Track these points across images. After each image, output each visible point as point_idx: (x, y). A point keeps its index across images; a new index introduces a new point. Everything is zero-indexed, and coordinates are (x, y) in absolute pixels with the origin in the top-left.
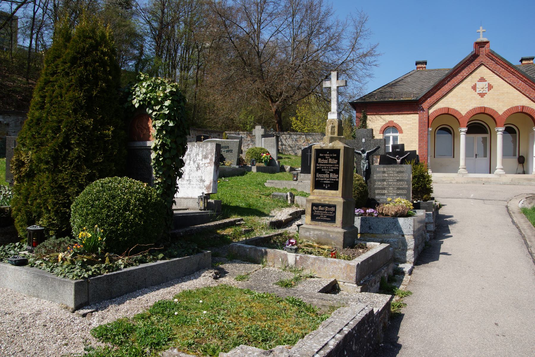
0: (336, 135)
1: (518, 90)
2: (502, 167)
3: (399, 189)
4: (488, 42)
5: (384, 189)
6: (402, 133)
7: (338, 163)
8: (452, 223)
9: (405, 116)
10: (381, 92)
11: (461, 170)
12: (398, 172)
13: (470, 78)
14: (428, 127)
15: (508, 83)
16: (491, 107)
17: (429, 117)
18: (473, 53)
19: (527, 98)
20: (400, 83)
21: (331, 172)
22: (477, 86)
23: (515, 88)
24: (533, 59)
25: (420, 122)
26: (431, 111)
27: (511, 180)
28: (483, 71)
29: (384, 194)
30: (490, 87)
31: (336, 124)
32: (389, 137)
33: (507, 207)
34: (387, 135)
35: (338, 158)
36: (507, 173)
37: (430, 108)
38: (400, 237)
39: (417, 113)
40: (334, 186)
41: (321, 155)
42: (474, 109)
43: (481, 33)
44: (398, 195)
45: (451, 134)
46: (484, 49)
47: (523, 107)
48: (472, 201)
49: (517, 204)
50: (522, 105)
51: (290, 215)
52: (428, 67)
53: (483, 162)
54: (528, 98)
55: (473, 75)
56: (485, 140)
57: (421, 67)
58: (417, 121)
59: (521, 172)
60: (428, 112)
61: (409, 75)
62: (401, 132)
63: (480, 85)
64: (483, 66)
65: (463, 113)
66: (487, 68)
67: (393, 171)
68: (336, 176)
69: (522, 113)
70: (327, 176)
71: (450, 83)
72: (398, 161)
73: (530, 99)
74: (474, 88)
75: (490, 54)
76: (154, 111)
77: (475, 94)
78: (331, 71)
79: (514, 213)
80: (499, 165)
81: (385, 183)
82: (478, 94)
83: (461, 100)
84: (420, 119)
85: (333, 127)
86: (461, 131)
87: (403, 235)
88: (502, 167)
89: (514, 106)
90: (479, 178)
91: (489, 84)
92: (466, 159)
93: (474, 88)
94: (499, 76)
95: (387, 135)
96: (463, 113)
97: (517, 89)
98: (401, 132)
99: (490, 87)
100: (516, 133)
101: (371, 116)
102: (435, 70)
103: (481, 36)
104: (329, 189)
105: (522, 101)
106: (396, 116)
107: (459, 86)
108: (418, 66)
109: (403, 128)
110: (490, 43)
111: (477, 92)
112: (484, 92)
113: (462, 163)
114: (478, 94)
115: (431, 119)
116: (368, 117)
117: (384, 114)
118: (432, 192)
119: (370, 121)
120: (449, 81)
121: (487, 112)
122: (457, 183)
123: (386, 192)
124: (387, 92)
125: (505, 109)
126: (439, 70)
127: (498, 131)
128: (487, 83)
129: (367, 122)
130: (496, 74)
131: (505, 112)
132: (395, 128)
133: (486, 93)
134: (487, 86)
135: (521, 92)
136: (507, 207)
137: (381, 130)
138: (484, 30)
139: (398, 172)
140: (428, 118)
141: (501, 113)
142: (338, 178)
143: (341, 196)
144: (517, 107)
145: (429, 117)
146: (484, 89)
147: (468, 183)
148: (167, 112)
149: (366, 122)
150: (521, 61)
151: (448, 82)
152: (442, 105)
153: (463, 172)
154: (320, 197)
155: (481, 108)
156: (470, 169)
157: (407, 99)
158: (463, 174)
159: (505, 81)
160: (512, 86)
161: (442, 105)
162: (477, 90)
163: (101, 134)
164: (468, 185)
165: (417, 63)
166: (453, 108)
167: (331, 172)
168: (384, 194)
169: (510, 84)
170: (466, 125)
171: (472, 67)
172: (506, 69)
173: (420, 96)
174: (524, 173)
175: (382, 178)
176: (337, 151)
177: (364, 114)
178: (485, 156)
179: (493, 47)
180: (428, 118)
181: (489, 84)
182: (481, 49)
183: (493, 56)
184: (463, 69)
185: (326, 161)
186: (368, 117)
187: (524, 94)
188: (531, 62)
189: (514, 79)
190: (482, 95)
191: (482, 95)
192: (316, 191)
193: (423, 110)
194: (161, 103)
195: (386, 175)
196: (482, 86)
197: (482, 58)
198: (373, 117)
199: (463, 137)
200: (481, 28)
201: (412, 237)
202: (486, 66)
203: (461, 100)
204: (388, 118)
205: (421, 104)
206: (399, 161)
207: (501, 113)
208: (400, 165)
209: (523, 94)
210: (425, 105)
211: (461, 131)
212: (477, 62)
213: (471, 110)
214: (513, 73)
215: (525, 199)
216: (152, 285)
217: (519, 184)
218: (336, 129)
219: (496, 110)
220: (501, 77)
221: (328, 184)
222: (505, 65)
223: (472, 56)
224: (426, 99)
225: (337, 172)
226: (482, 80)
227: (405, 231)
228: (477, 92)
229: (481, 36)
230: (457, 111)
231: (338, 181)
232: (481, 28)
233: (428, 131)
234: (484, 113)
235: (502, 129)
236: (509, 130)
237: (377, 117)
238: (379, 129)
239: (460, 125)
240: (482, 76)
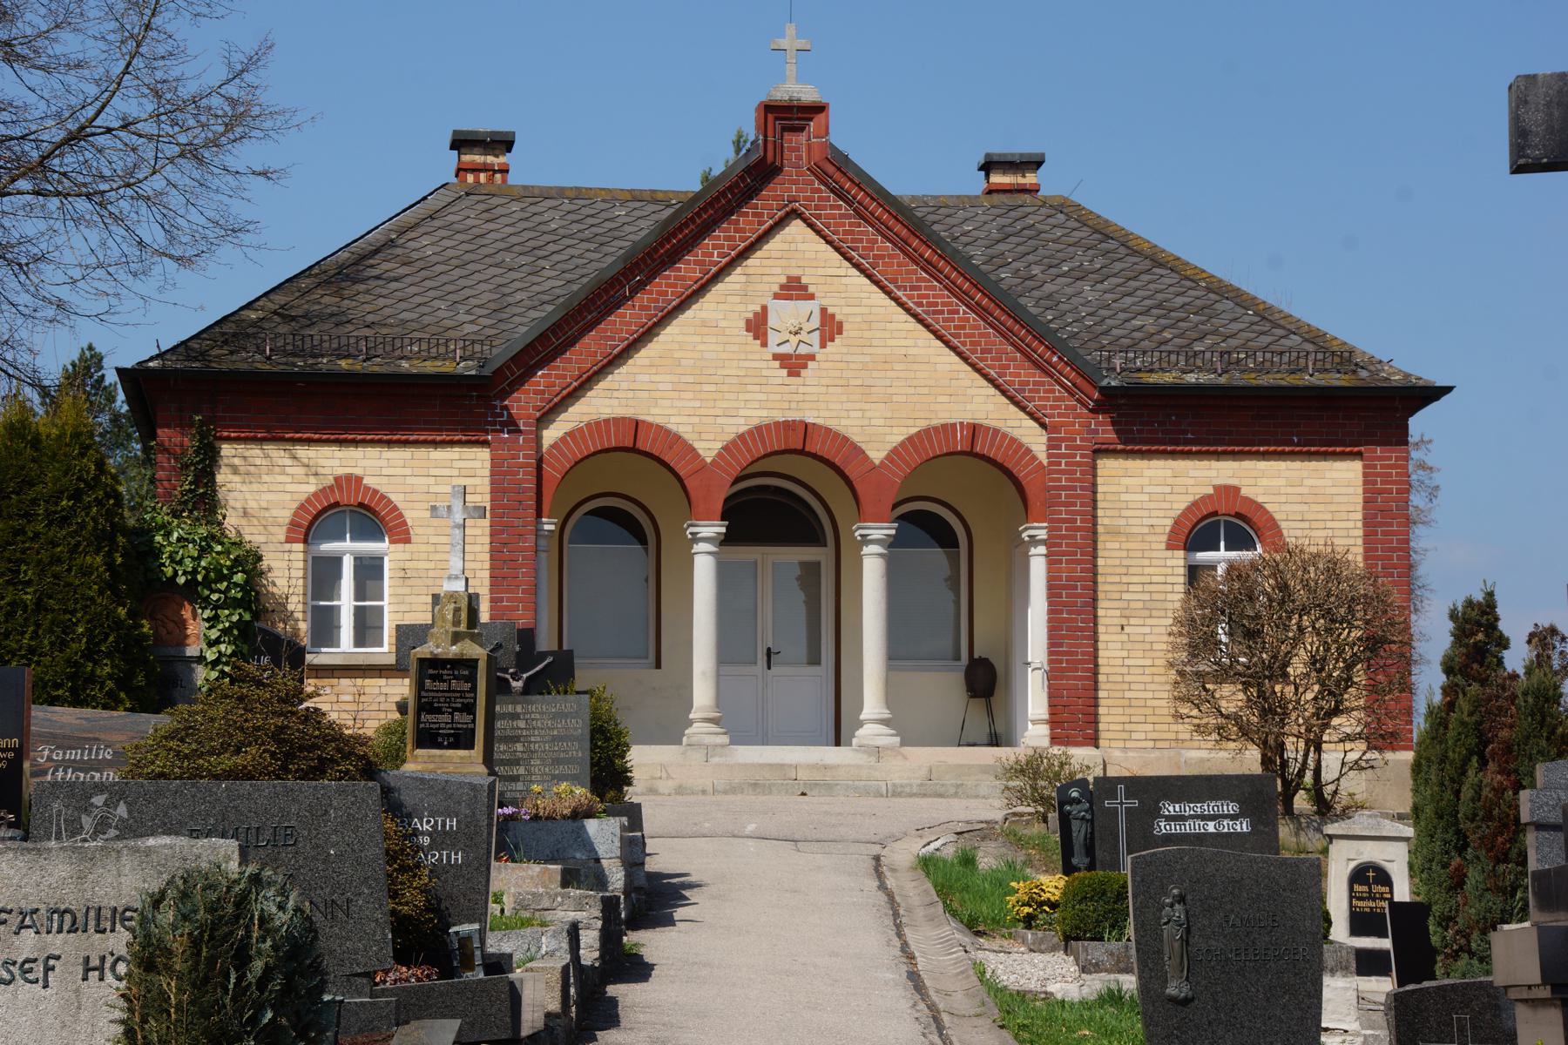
0: (463, 628)
1: (954, 349)
2: (886, 714)
3: (557, 762)
4: (819, 109)
5: (517, 762)
6: (407, 541)
7: (474, 689)
8: (691, 886)
9: (421, 453)
10: (283, 314)
11: (699, 731)
12: (554, 717)
13: (736, 278)
14: (539, 515)
15: (908, 310)
16: (831, 424)
17: (540, 461)
18: (754, 157)
19: (992, 391)
21: (456, 710)
22: (772, 321)
23: (940, 337)
24: (1035, 163)
25: (498, 487)
26: (551, 435)
27: (924, 773)
28: (796, 249)
29: (515, 779)
30: (830, 327)
31: (464, 604)
32: (336, 561)
33: (877, 858)
34: (328, 547)
35: (472, 679)
36: (910, 738)
37: (547, 415)
38: (592, 864)
39: (485, 443)
40: (462, 740)
41: (431, 671)
42: (759, 428)
43: (791, 56)
44: (560, 778)
45: (643, 540)
46: (803, 137)
47: (974, 429)
48: (750, 842)
49: (904, 854)
50: (968, 418)
52: (524, 168)
53: (803, 686)
54: (997, 387)
55: (752, 262)
56: (810, 573)
57: (485, 168)
59: (985, 739)
60: (539, 439)
61: (422, 217)
62: (401, 534)
63: (785, 315)
64: (798, 222)
65: (708, 449)
66: (818, 232)
67: (542, 713)
68: (467, 718)
69: (969, 453)
70: (446, 718)
71: (642, 298)
72: (514, 684)
73: (1004, 393)
74: (758, 326)
75: (830, 169)
76: (213, 591)
77: (760, 360)
79: (893, 870)
80: (872, 702)
81: (519, 747)
82: (776, 357)
83: (697, 381)
84: (498, 475)
85: (457, 610)
86: (696, 539)
87: (598, 860)
88: (886, 714)
89: (936, 422)
90: (782, 766)
91: (824, 311)
92: (719, 676)
93: (758, 326)
94: (869, 276)
95: (328, 547)
96: (708, 449)
97: (947, 343)
98: (401, 534)
99: (830, 327)
100: (956, 545)
101: (241, 448)
102: (561, 192)
103: (791, 70)
104: (455, 746)
105: (980, 404)
106: (372, 452)
107: (689, 314)
108: (467, 158)
109: (410, 516)
110: (832, 110)
111: (773, 348)
112: (803, 350)
113: (703, 693)
114: (776, 357)
115: (552, 472)
116: (226, 450)
117: (309, 441)
118: (629, 782)
119: (235, 470)
120: (641, 285)
121: (815, 446)
122: (680, 790)
123: (522, 771)
124: (322, 318)
125: (897, 436)
126: (578, 194)
127: (865, 540)
128: (813, 306)
129: (219, 478)
130: (857, 266)
131: (894, 451)
132: (369, 515)
133: (812, 357)
134: (816, 322)
135: (965, 359)
136: (877, 858)
137: (293, 525)
138: (801, 43)
139: (554, 717)
140: (539, 469)
141: (877, 455)
142: (474, 721)
143: (481, 760)
144: (948, 429)
145: (540, 461)
146: (803, 336)
147: (732, 790)
148: (239, 595)
149: (212, 476)
150: (988, 167)
151: (634, 291)
153: (709, 740)
154: (431, 766)
155: (788, 426)
156: (742, 724)
157: (430, 367)
158: (709, 750)
159: (897, 300)
160: (927, 326)
161: (602, 403)
162: (773, 338)
164: (730, 797)
165: (461, 143)
166: (658, 420)
167: (456, 710)
168: (515, 779)
169: (915, 316)
170: (719, 506)
171: (746, 222)
172: (902, 245)
173: (500, 353)
174: (995, 741)
175: (509, 733)
176: (472, 664)
177: (203, 436)
178: (814, 659)
179: (845, 133)
180: (539, 469)
181: (824, 311)
182: (792, 140)
183: (840, 174)
184: (706, 229)
185: (444, 686)
186: (226, 450)
187: (978, 370)
188: (1030, 179)
189: (937, 293)
190: (793, 364)
191: (793, 364)
192: (419, 752)
193: (511, 425)
194: (228, 578)
195: (522, 724)
196: (792, 323)
197: (792, 185)
198: (254, 452)
199: (704, 569)
200: (791, 30)
201: (618, 862)
202: (811, 226)
203: (697, 381)
204: (334, 461)
205: (505, 394)
206: (517, 685)
207: (877, 455)
208: (522, 698)
209: (973, 366)
210: (523, 403)
211: (696, 539)
212: (768, 202)
213: (741, 437)
214: (927, 266)
215: (953, 838)
217: (959, 792)
218: (464, 615)
219: (855, 438)
220: (877, 283)
221: (449, 735)
222: (898, 228)
223: (748, 170)
224: (530, 372)
225: (470, 709)
226: (794, 289)
227: (601, 850)
228: (773, 348)
229: (791, 70)
230: (675, 439)
231: (473, 731)
232: (791, 30)
233: (538, 531)
234: (802, 452)
235: (880, 531)
236: (926, 526)
237: (276, 453)
238: (285, 515)
239: (690, 508)
240: (795, 272)
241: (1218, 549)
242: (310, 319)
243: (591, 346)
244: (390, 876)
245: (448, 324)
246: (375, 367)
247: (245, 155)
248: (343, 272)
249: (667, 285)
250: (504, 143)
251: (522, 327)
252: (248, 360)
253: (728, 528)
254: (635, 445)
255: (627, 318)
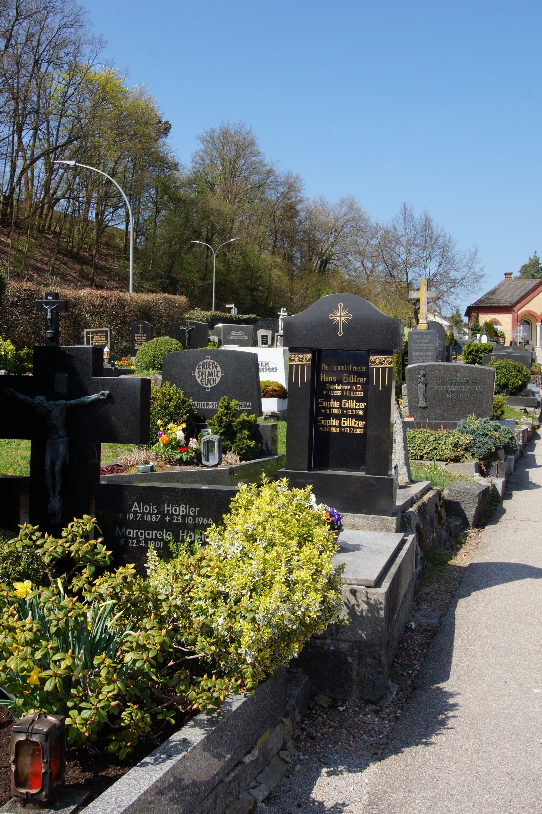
20: (497, 291)
26: (519, 312)
37: (519, 310)
51: (402, 752)
58: (511, 318)
62: (501, 325)
78: (427, 334)
96: (539, 314)
98: (501, 325)
152: (526, 308)
161: (526, 308)
163: (187, 750)
165: (506, 274)
173: (513, 302)
210: (516, 309)
216: (185, 202)
230: (535, 313)
239: (537, 321)
241: (124, 287)
242: (489, 299)
243: (524, 301)
244: (246, 584)
245: (505, 299)
246: (498, 305)
247: (482, 280)
248: (493, 292)
249: (534, 294)
250: (511, 274)
251: (516, 299)
252: (483, 305)
253: (97, 469)
254: (530, 313)
255: (529, 298)
